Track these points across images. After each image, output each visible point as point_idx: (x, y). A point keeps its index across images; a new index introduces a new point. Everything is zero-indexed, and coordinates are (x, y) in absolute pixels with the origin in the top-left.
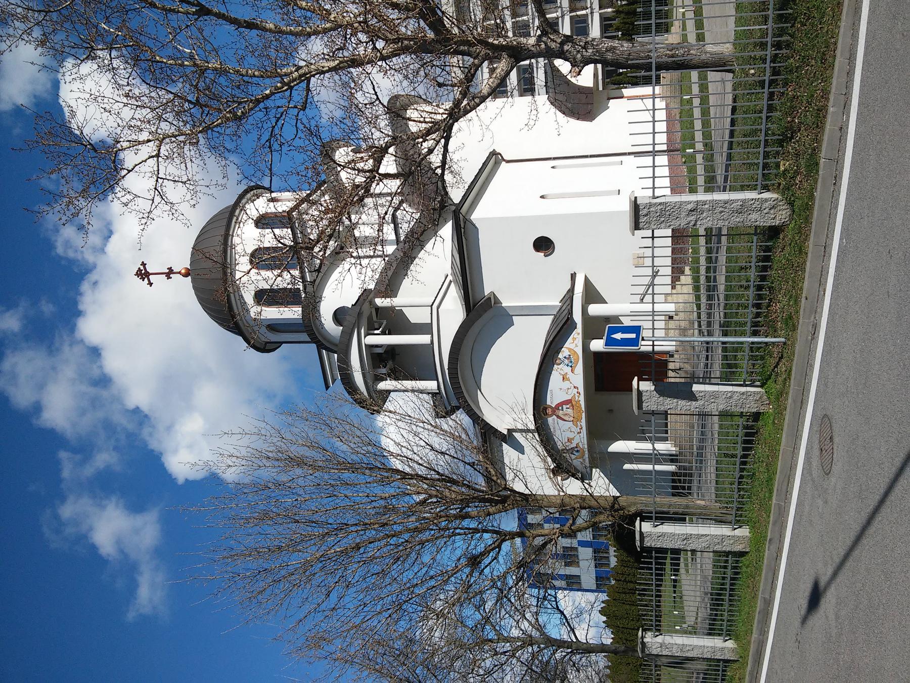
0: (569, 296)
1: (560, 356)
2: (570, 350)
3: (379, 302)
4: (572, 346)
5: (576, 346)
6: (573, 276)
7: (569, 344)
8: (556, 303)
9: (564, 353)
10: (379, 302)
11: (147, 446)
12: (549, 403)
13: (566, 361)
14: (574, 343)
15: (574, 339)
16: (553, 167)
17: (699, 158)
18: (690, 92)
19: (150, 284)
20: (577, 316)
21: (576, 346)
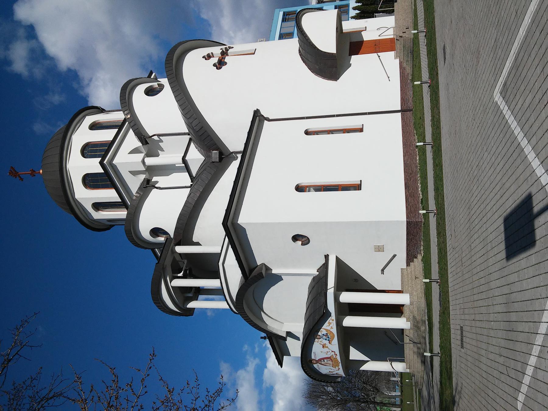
0: (324, 268)
1: (319, 334)
2: (327, 330)
3: (180, 249)
4: (329, 328)
5: (332, 328)
6: (327, 257)
7: (326, 326)
8: (314, 272)
9: (322, 332)
10: (180, 249)
11: (55, 66)
12: (313, 357)
13: (325, 337)
14: (330, 326)
15: (330, 323)
16: (307, 133)
17: (429, 149)
18: (420, 79)
19: (22, 179)
20: (331, 306)
21: (332, 328)
